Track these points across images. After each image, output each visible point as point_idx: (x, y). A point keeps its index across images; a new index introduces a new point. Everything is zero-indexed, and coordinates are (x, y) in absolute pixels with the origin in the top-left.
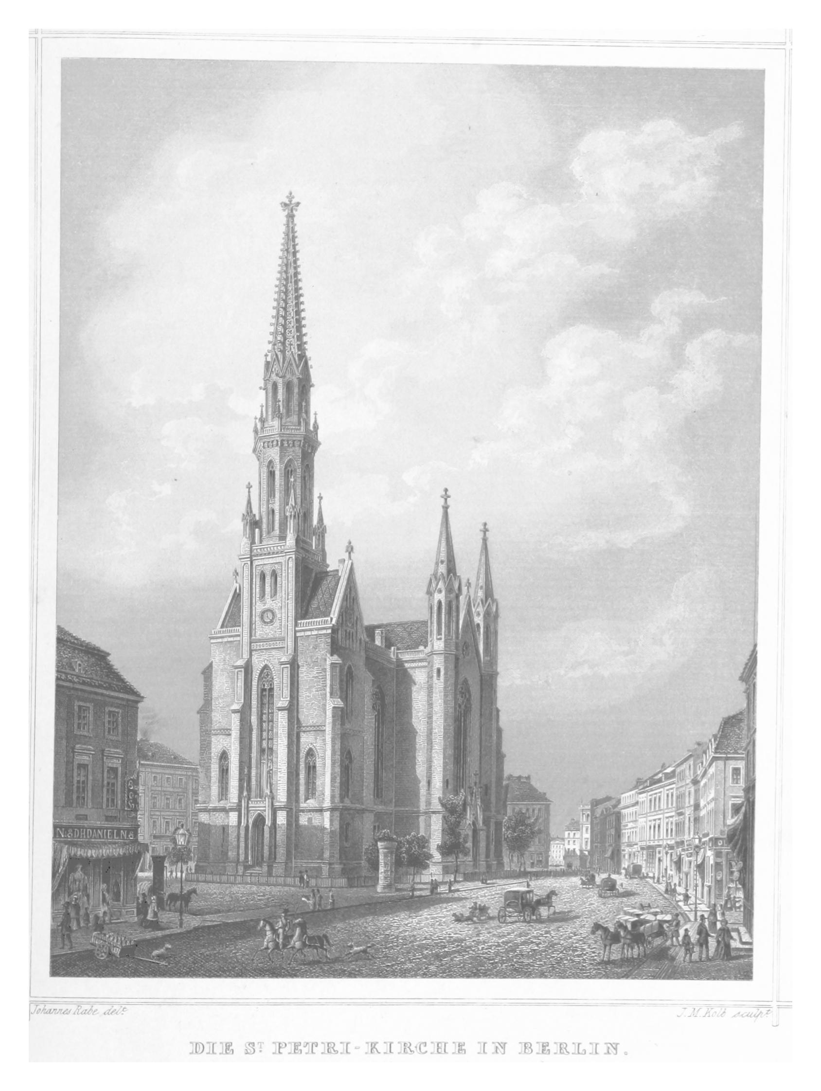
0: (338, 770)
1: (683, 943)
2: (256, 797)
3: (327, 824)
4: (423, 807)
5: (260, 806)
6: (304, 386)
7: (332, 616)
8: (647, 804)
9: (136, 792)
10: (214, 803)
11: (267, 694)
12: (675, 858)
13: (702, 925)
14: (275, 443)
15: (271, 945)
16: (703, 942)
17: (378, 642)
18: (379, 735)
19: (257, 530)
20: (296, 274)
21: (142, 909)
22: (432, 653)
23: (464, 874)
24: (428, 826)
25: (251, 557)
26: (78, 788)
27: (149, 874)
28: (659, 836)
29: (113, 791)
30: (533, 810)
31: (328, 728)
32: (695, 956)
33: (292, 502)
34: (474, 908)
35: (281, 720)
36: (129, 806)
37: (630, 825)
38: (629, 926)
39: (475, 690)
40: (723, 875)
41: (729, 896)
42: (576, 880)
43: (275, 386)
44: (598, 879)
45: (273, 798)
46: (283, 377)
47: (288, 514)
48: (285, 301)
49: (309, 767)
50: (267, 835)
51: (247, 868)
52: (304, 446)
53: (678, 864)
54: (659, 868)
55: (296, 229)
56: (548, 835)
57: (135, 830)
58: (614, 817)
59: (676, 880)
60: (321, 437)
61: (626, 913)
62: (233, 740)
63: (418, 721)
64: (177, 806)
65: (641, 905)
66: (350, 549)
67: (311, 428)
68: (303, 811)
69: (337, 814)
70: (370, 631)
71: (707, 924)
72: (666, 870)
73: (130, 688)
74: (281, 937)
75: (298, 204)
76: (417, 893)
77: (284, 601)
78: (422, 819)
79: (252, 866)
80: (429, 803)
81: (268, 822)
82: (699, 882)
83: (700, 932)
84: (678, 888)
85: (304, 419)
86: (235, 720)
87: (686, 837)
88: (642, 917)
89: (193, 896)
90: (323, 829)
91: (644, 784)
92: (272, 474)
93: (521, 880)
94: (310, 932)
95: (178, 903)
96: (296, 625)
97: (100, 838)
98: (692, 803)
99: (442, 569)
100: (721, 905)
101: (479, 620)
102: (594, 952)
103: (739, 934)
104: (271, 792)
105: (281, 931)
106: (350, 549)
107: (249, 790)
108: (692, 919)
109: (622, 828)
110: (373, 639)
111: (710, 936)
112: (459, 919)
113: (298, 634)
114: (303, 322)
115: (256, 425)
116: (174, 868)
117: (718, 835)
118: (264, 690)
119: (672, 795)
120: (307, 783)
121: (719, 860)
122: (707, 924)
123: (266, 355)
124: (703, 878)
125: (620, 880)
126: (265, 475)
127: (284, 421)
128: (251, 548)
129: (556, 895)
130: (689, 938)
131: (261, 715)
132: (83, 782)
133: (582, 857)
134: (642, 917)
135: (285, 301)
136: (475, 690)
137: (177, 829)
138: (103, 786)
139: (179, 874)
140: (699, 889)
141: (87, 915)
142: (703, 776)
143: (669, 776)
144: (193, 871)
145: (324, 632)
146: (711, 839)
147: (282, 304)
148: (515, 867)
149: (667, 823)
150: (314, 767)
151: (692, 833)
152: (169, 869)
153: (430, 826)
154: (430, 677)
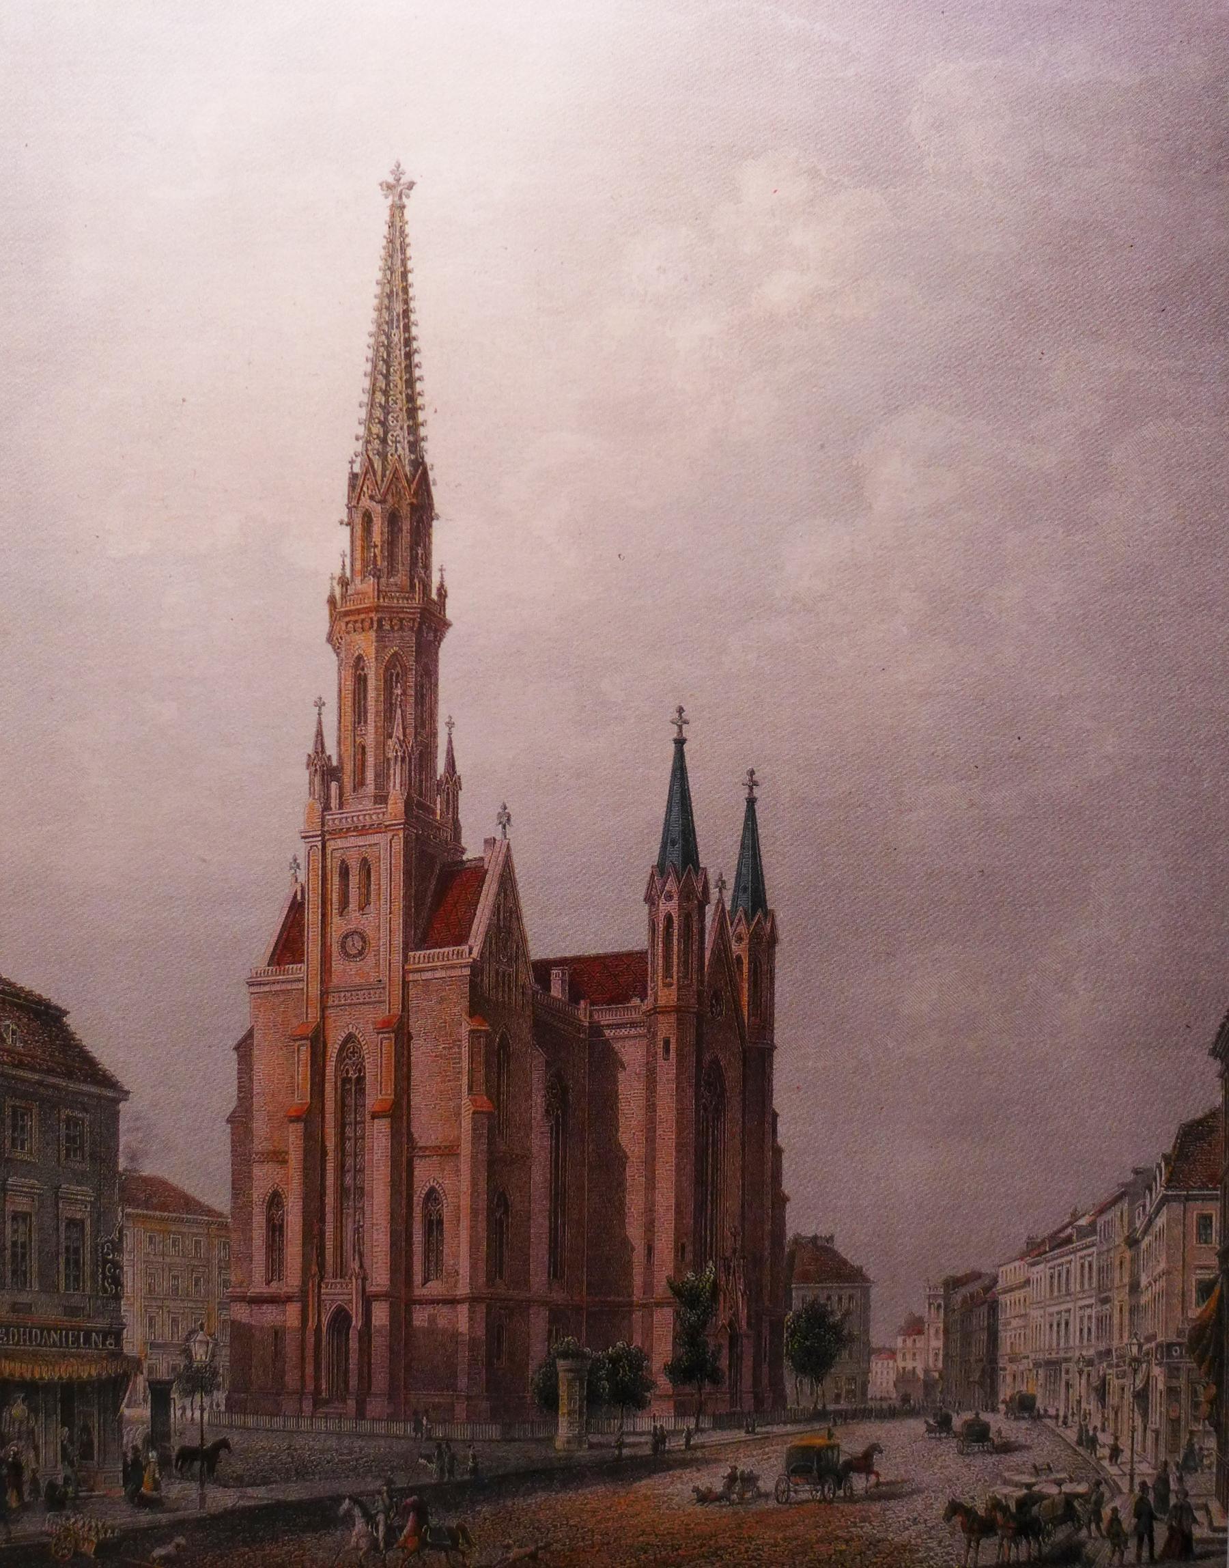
0: (482, 1225)
1: (1109, 1532)
2: (335, 1277)
3: (463, 1326)
4: (637, 1296)
5: (340, 1293)
6: (420, 520)
7: (471, 941)
8: (1045, 1283)
9: (117, 1265)
10: (258, 1287)
11: (353, 1086)
12: (1095, 1382)
13: (1142, 1501)
14: (367, 624)
15: (364, 1543)
16: (1144, 1532)
17: (556, 991)
18: (557, 1165)
19: (334, 785)
20: (406, 313)
21: (133, 1472)
22: (655, 1011)
23: (714, 1415)
24: (648, 1332)
25: (323, 835)
26: (14, 1255)
27: (145, 1412)
28: (1067, 1341)
29: (77, 1262)
30: (840, 1299)
31: (466, 1149)
32: (1130, 1556)
33: (398, 732)
34: (732, 1478)
35: (378, 1136)
36: (105, 1291)
37: (1015, 1323)
38: (1013, 1508)
39: (733, 1074)
40: (1184, 1409)
41: (1190, 1444)
42: (917, 1426)
43: (367, 518)
44: (957, 1422)
45: (364, 1279)
46: (382, 502)
47: (391, 755)
48: (387, 363)
49: (431, 1222)
50: (354, 1344)
51: (316, 1404)
52: (420, 628)
53: (1101, 1391)
54: (1067, 1399)
55: (408, 229)
56: (867, 1343)
57: (115, 1333)
58: (984, 1309)
59: (1097, 1421)
60: (450, 614)
61: (1006, 1482)
62: (291, 1171)
63: (629, 1137)
64: (192, 1290)
65: (1035, 1467)
66: (505, 819)
67: (434, 596)
68: (420, 1302)
69: (482, 1308)
70: (543, 969)
71: (1151, 1497)
72: (1079, 1402)
73: (104, 1076)
74: (381, 1528)
75: (411, 185)
76: (626, 1451)
77: (383, 916)
78: (637, 1315)
79: (327, 1402)
80: (648, 1287)
81: (357, 1322)
82: (1138, 1422)
83: (1138, 1514)
84: (1100, 1435)
85: (421, 580)
86: (293, 1138)
87: (1115, 1343)
88: (1036, 1488)
89: (223, 1453)
90: (455, 1335)
91: (1036, 1250)
92: (361, 681)
93: (817, 1426)
94: (434, 1521)
95: (197, 1464)
96: (406, 959)
97: (54, 1345)
98: (1126, 1280)
99: (675, 855)
100: (1177, 1464)
101: (738, 949)
102: (948, 1554)
103: (1208, 1512)
104: (361, 1266)
105: (381, 1517)
106: (505, 819)
107: (322, 1266)
108: (1125, 1490)
109: (1000, 1328)
110: (547, 987)
111: (1156, 1518)
112: (704, 1497)
113: (411, 977)
114: (420, 401)
115: (333, 589)
116: (187, 1402)
117: (1174, 1339)
118: (346, 1081)
119: (1090, 1266)
120: (427, 1251)
121: (1174, 1383)
122: (1151, 1497)
123: (352, 462)
124: (1145, 1415)
125: (1000, 1423)
126: (350, 684)
127: (383, 580)
128: (323, 818)
129: (881, 1452)
130: (1119, 1522)
131: (342, 1126)
132: (23, 1246)
133: (928, 1386)
134: (1036, 1488)
135: (387, 363)
136: (733, 1074)
137: (193, 1332)
138: (58, 1254)
139: (197, 1414)
140: (1138, 1436)
141: (34, 1481)
142: (1145, 1232)
143: (1084, 1233)
144: (223, 1408)
145: (457, 972)
146: (1159, 1346)
147: (382, 366)
148: (806, 1404)
149: (1081, 1319)
150: (440, 1222)
151: (1126, 1335)
152: (179, 1404)
153: (651, 1328)
154: (651, 1054)
